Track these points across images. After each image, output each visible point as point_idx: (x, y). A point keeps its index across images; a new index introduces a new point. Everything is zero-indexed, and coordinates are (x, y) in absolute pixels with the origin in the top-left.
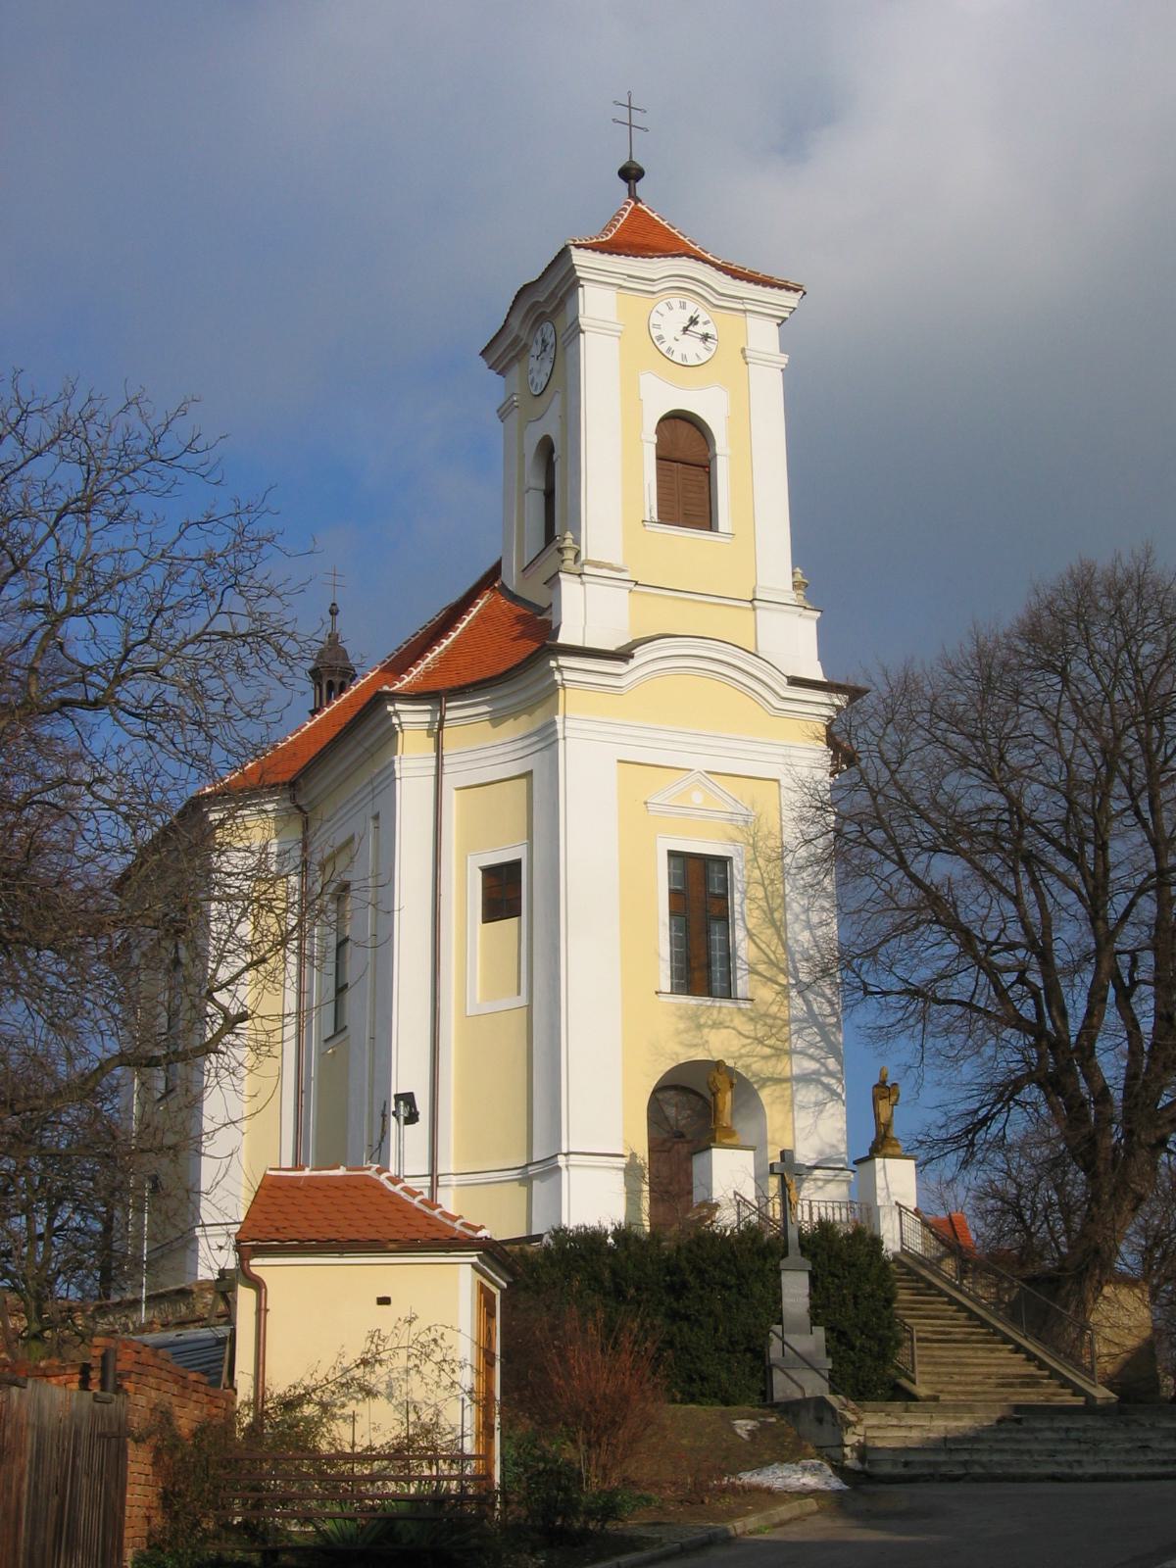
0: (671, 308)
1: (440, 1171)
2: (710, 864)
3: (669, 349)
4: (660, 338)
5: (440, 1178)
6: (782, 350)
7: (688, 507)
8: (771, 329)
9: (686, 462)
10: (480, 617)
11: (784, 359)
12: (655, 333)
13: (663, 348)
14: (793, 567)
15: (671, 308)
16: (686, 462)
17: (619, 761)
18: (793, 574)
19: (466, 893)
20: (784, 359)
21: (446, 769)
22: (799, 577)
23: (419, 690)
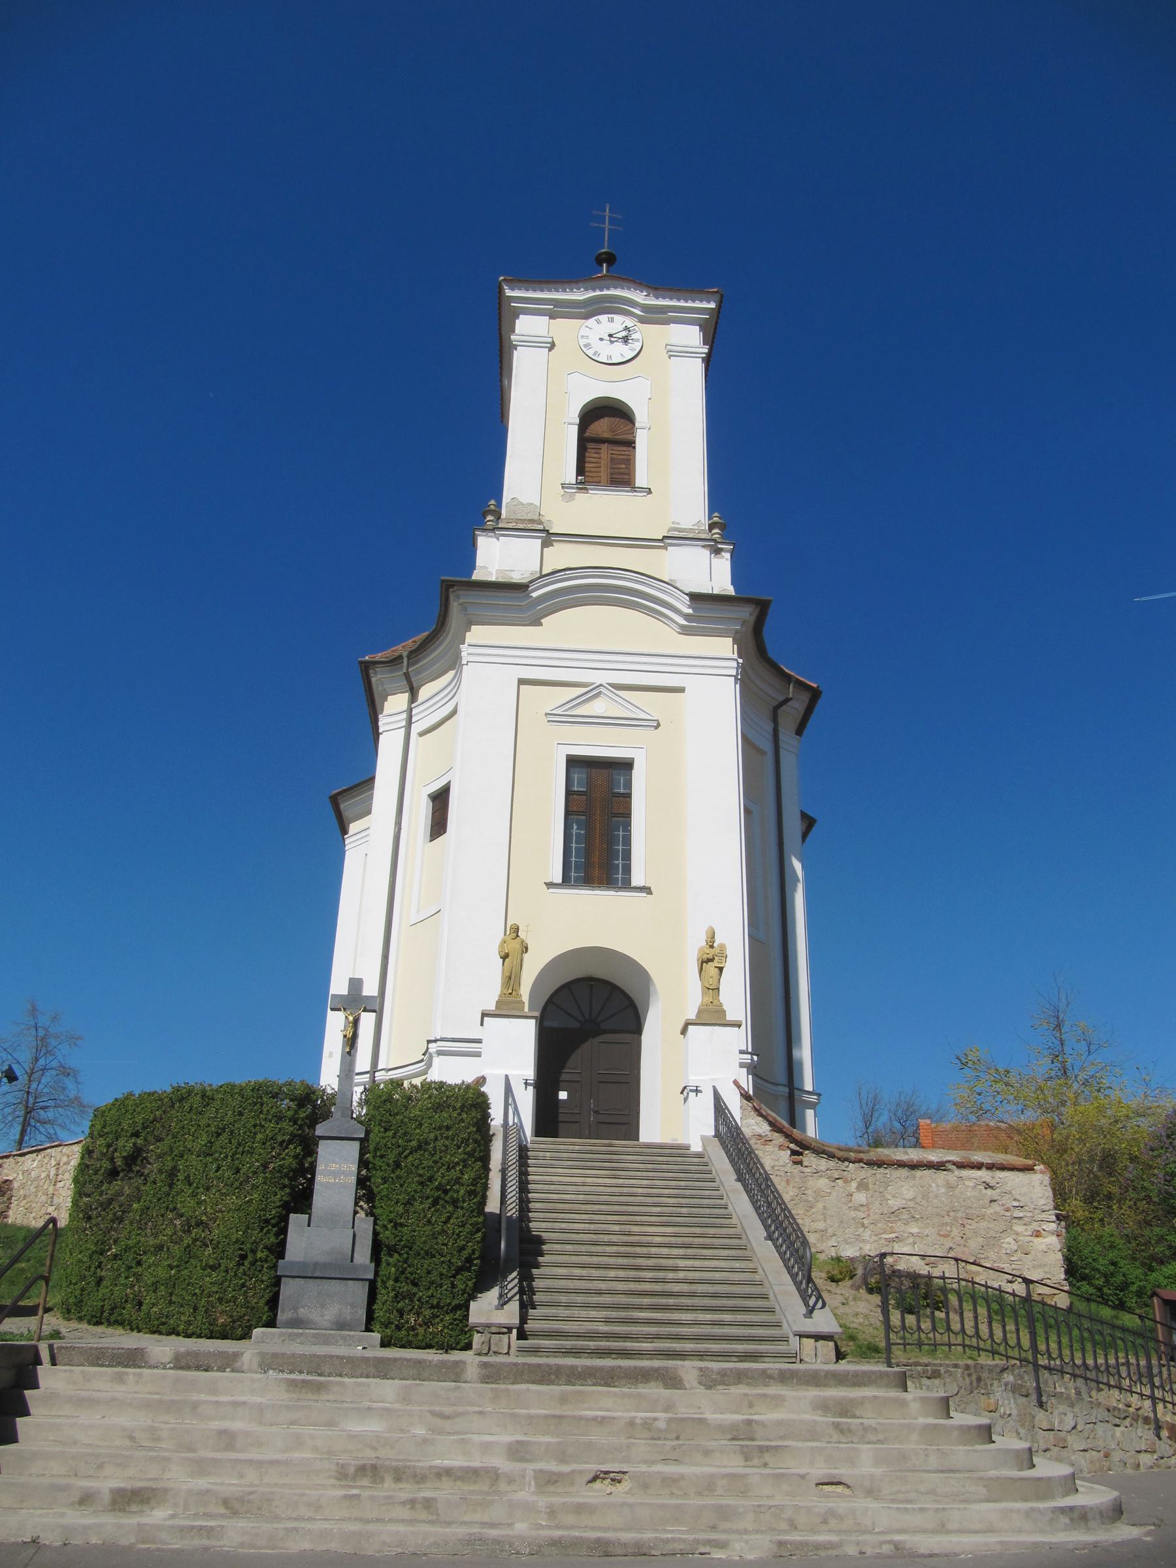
2: (560, 881)
3: (595, 353)
4: (588, 346)
12: (582, 342)
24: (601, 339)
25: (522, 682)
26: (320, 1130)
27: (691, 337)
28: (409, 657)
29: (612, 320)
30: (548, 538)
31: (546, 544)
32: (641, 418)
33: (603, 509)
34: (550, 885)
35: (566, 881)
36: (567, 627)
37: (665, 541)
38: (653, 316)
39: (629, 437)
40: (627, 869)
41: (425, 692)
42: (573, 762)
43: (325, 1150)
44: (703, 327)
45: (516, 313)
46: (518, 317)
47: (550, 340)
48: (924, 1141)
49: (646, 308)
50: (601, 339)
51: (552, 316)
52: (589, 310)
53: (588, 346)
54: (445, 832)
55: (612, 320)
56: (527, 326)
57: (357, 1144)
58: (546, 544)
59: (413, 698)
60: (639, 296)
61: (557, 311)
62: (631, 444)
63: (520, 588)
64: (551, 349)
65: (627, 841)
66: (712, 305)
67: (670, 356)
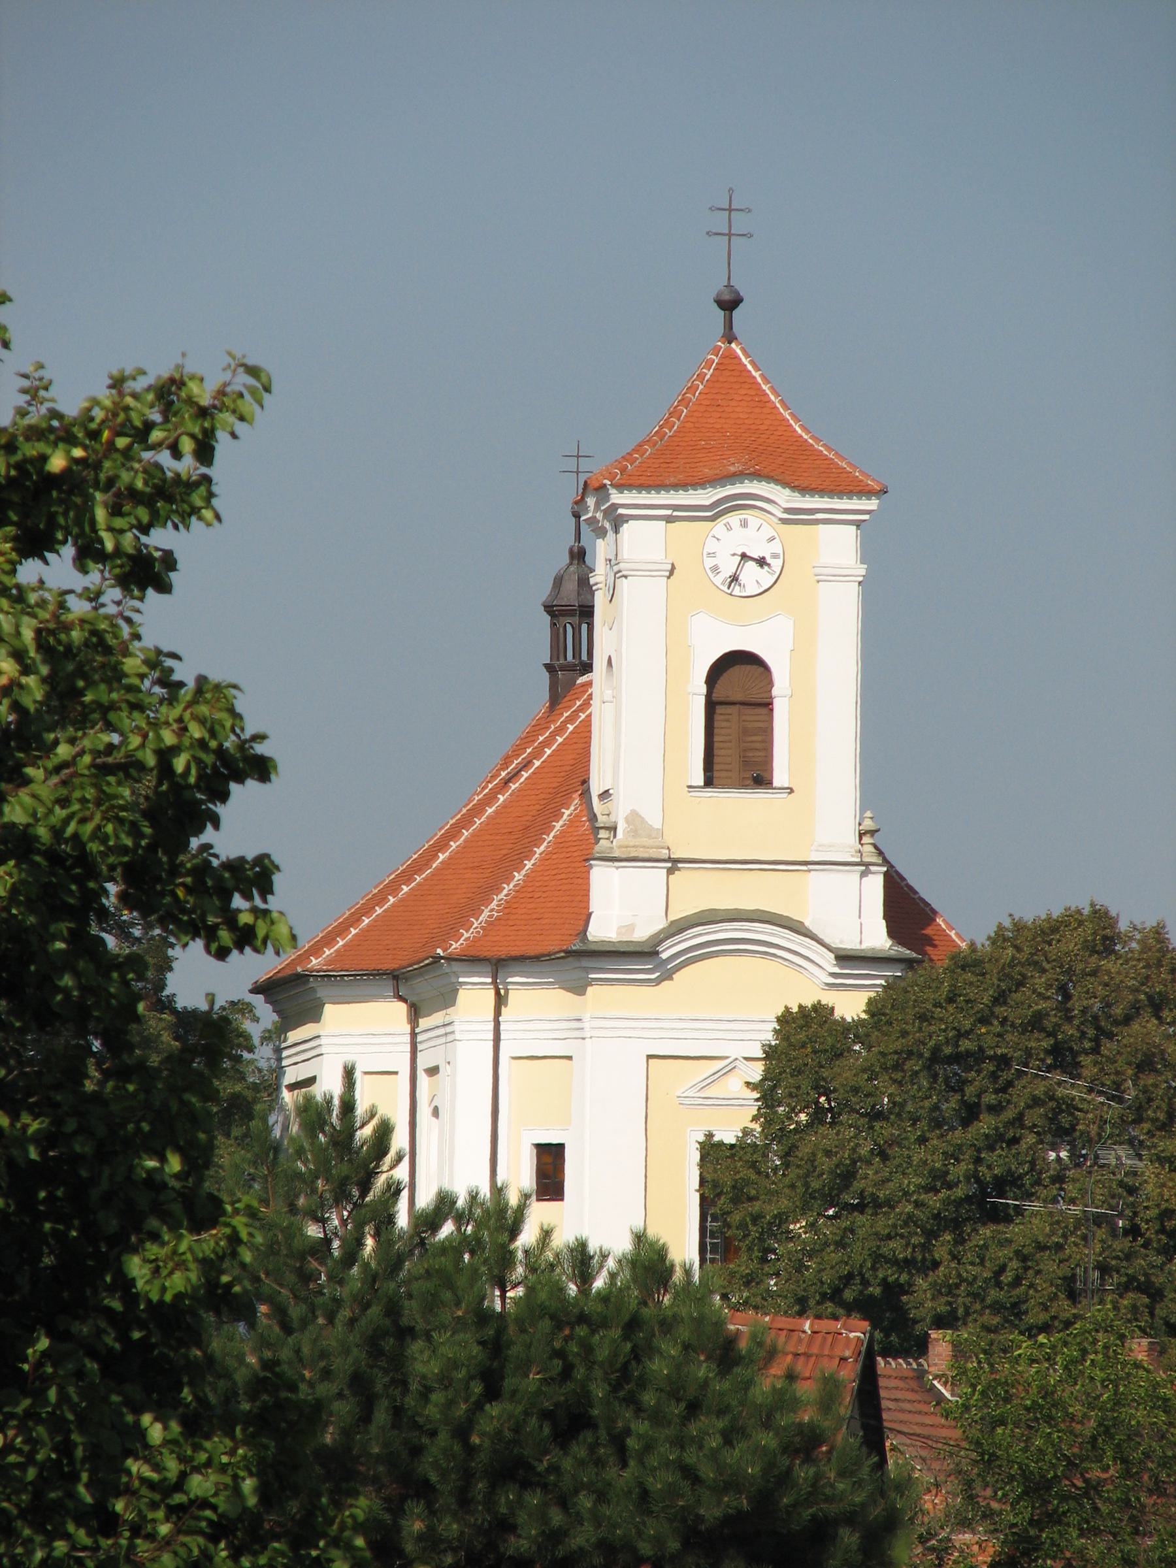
14: (863, 810)
15: (729, 528)
20: (862, 570)
22: (868, 824)
29: (744, 524)
38: (794, 517)
51: (669, 520)
52: (717, 511)
55: (744, 524)
59: (500, 1001)
60: (784, 497)
64: (669, 577)
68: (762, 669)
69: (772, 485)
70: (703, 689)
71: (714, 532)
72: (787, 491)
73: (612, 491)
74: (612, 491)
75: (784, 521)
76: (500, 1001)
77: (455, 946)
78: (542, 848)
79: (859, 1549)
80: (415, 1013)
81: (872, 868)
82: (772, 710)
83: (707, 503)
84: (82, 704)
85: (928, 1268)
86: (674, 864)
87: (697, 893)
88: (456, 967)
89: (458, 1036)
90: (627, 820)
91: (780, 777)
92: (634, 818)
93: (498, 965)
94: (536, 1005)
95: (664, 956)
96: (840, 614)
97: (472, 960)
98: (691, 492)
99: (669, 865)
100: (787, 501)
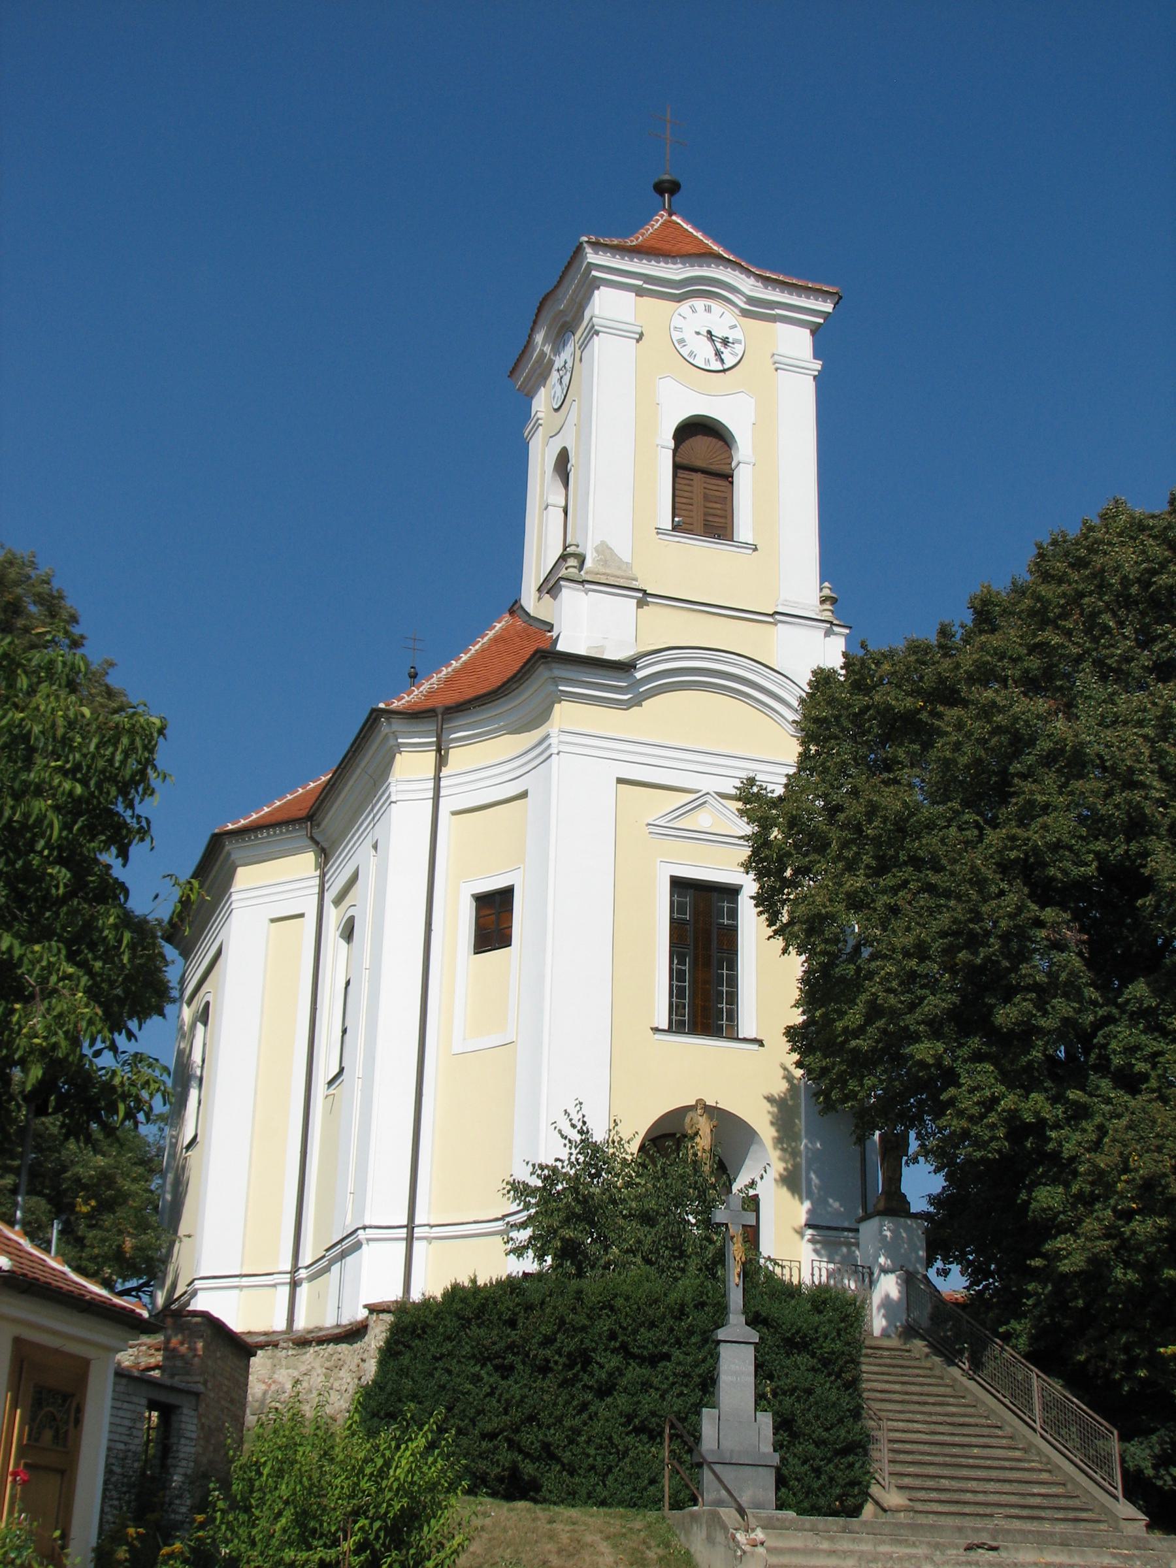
0: (694, 311)
1: (417, 1222)
2: (666, 1027)
3: (691, 353)
4: (682, 341)
5: (416, 1230)
6: (816, 357)
7: (710, 518)
8: (805, 335)
9: (702, 461)
10: (496, 640)
11: (817, 365)
12: (676, 336)
13: (685, 352)
14: (821, 582)
15: (694, 311)
16: (702, 461)
17: (273, 921)
18: (821, 590)
19: (457, 921)
20: (817, 365)
21: (443, 792)
22: (827, 592)
23: (417, 708)
24: (698, 333)
25: (620, 781)
26: (721, 1334)
27: (797, 343)
28: (443, 714)
29: (708, 309)
30: (644, 598)
31: (641, 604)
32: (744, 449)
33: (695, 564)
34: (656, 1030)
35: (676, 1026)
36: (666, 713)
37: (776, 617)
38: (757, 310)
39: (724, 469)
40: (732, 1016)
41: (456, 756)
42: (678, 884)
43: (725, 1351)
44: (815, 330)
45: (596, 284)
46: (598, 288)
47: (639, 330)
48: (687, 1285)
49: (751, 300)
50: (698, 333)
51: (640, 292)
52: (685, 291)
53: (682, 341)
54: (510, 945)
55: (708, 309)
56: (608, 305)
57: (752, 1347)
58: (641, 604)
59: (441, 761)
60: (748, 285)
61: (646, 288)
62: (727, 477)
63: (625, 667)
64: (638, 341)
65: (733, 981)
66: (828, 307)
67: (777, 369)
68: (721, 443)
69: (737, 273)
70: (672, 444)
71: (679, 311)
72: (752, 281)
73: (588, 250)
74: (588, 250)
75: (745, 313)
76: (441, 761)
77: (396, 705)
78: (477, 647)
79: (909, 1332)
80: (325, 855)
81: (836, 629)
82: (732, 483)
83: (677, 278)
84: (88, 1123)
85: (1016, 935)
86: (644, 598)
87: (666, 628)
88: (397, 725)
89: (393, 798)
90: (596, 550)
91: (744, 526)
92: (604, 550)
93: (442, 718)
94: (483, 760)
95: (639, 675)
96: (798, 401)
97: (416, 715)
98: (662, 264)
99: (640, 595)
100: (751, 290)
